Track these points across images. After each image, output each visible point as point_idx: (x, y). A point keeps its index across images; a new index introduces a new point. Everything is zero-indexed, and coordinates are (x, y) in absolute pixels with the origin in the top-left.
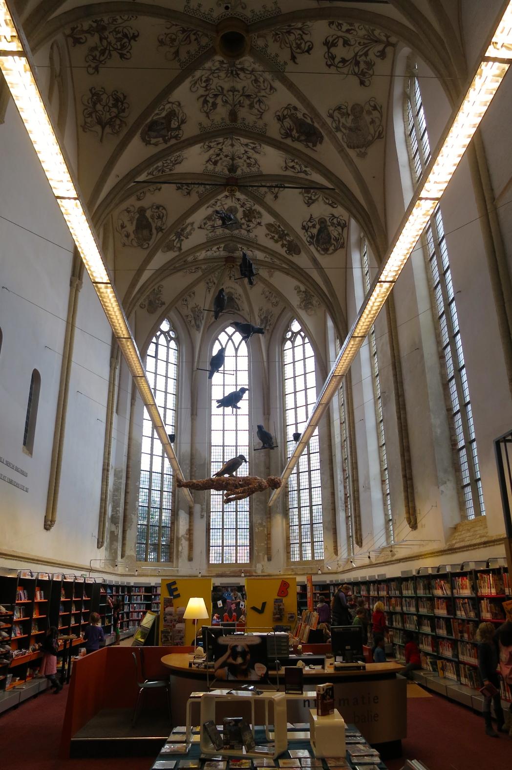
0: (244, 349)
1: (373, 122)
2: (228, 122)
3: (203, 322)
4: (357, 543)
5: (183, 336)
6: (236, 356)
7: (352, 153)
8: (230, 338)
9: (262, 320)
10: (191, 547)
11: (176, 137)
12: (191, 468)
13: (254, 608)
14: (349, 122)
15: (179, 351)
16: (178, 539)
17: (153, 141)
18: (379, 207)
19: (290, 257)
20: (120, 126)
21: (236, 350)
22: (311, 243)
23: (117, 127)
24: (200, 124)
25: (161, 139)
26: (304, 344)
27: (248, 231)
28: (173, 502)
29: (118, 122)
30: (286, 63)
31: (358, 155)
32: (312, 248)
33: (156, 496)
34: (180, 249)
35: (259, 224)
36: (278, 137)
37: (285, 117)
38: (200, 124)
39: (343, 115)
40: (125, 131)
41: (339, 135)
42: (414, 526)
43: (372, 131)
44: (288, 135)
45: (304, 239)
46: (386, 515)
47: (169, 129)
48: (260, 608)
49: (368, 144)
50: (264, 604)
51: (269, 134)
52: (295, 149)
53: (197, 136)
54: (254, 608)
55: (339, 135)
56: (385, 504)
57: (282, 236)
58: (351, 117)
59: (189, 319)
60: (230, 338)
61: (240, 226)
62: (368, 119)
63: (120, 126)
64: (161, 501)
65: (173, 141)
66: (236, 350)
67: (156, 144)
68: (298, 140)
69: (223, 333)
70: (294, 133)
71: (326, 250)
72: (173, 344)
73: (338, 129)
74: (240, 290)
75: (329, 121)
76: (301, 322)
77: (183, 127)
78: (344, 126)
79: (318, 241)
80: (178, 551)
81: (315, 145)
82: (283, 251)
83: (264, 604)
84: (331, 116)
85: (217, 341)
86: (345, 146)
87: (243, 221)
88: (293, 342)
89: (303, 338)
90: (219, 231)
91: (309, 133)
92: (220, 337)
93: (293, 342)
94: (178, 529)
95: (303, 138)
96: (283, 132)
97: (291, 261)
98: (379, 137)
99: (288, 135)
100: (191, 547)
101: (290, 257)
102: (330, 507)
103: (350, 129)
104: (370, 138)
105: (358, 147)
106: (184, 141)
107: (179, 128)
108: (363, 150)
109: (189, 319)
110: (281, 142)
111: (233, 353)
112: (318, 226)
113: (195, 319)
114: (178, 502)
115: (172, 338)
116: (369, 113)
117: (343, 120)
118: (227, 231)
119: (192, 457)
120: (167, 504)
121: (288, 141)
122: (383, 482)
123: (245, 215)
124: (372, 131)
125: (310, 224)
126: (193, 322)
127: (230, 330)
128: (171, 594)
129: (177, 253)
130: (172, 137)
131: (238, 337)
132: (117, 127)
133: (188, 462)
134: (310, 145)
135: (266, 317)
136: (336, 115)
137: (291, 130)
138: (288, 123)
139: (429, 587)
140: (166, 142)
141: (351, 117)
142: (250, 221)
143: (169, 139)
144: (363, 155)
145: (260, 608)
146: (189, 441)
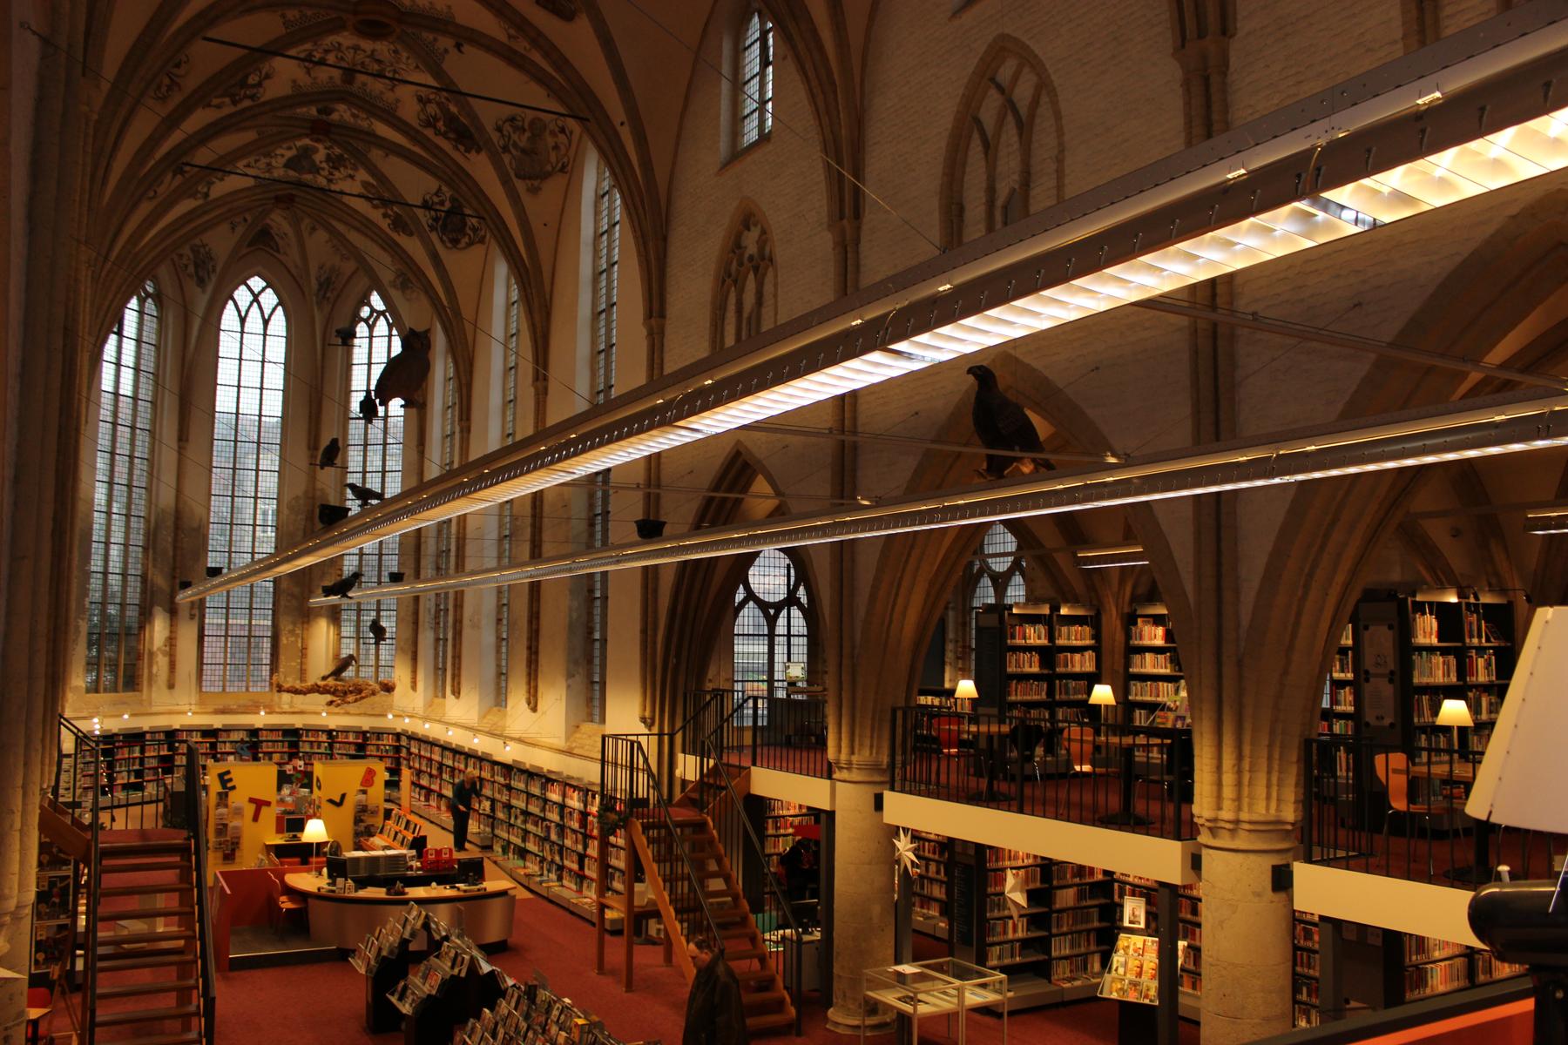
0: (279, 323)
1: (556, 147)
2: (339, 82)
3: (214, 278)
4: (453, 693)
5: (169, 290)
6: (265, 335)
7: (520, 185)
8: (256, 298)
9: (321, 285)
10: (172, 666)
11: (252, 97)
12: (176, 534)
13: (331, 801)
14: (523, 140)
15: (160, 319)
16: (151, 654)
17: (215, 101)
18: (546, 269)
19: (395, 236)
20: (169, 88)
21: (266, 322)
22: (432, 228)
23: (164, 89)
24: (294, 81)
25: (227, 100)
26: (390, 336)
27: (330, 181)
28: (143, 592)
29: (167, 81)
30: (446, 51)
31: (528, 190)
32: (434, 237)
33: (115, 581)
34: (206, 195)
35: (352, 177)
36: (415, 123)
37: (429, 101)
38: (294, 81)
39: (516, 129)
40: (177, 99)
41: (506, 158)
42: (534, 709)
43: (553, 159)
44: (430, 123)
45: (423, 221)
46: (499, 666)
47: (243, 84)
48: (337, 800)
49: (545, 176)
50: (343, 796)
51: (399, 113)
52: (437, 147)
53: (287, 97)
54: (331, 801)
55: (506, 158)
56: (498, 651)
57: (385, 203)
58: (527, 134)
59: (184, 261)
60: (256, 298)
61: (316, 170)
62: (551, 141)
63: (169, 88)
64: (124, 592)
65: (247, 103)
66: (266, 322)
67: (218, 107)
68: (444, 135)
69: (243, 288)
70: (440, 124)
71: (455, 242)
72: (150, 305)
73: (505, 149)
74: (286, 227)
75: (495, 136)
76: (385, 298)
77: (266, 83)
78: (515, 145)
79: (444, 227)
80: (150, 672)
81: (467, 150)
82: (385, 224)
83: (343, 796)
84: (499, 129)
85: (230, 303)
86: (512, 174)
87: (324, 165)
88: (371, 328)
89: (390, 326)
90: (278, 173)
91: (466, 136)
92: (237, 294)
93: (371, 328)
94: (152, 638)
95: (452, 135)
96: (423, 117)
97: (397, 244)
98: (563, 169)
99: (430, 123)
100: (172, 666)
101: (395, 236)
102: (410, 619)
103: (523, 151)
104: (549, 168)
105: (530, 178)
106: (264, 104)
107: (260, 84)
108: (536, 183)
109: (184, 261)
110: (418, 132)
111: (259, 328)
112: (448, 205)
113: (197, 266)
114: (152, 593)
115: (148, 295)
116: (553, 133)
117: (515, 137)
118: (292, 173)
119: (178, 514)
120: (134, 595)
121: (429, 132)
122: (499, 621)
123: (328, 158)
124: (553, 159)
125: (436, 199)
126: (191, 269)
127: (257, 283)
128: (224, 786)
129: (200, 202)
130: (246, 97)
131: (269, 299)
132: (164, 89)
133: (170, 523)
134: (462, 148)
135: (328, 279)
136: (507, 128)
137: (436, 119)
138: (432, 109)
139: (544, 787)
140: (234, 103)
141: (527, 134)
142: (337, 169)
143: (241, 100)
144: (534, 191)
145: (337, 800)
146: (174, 484)
